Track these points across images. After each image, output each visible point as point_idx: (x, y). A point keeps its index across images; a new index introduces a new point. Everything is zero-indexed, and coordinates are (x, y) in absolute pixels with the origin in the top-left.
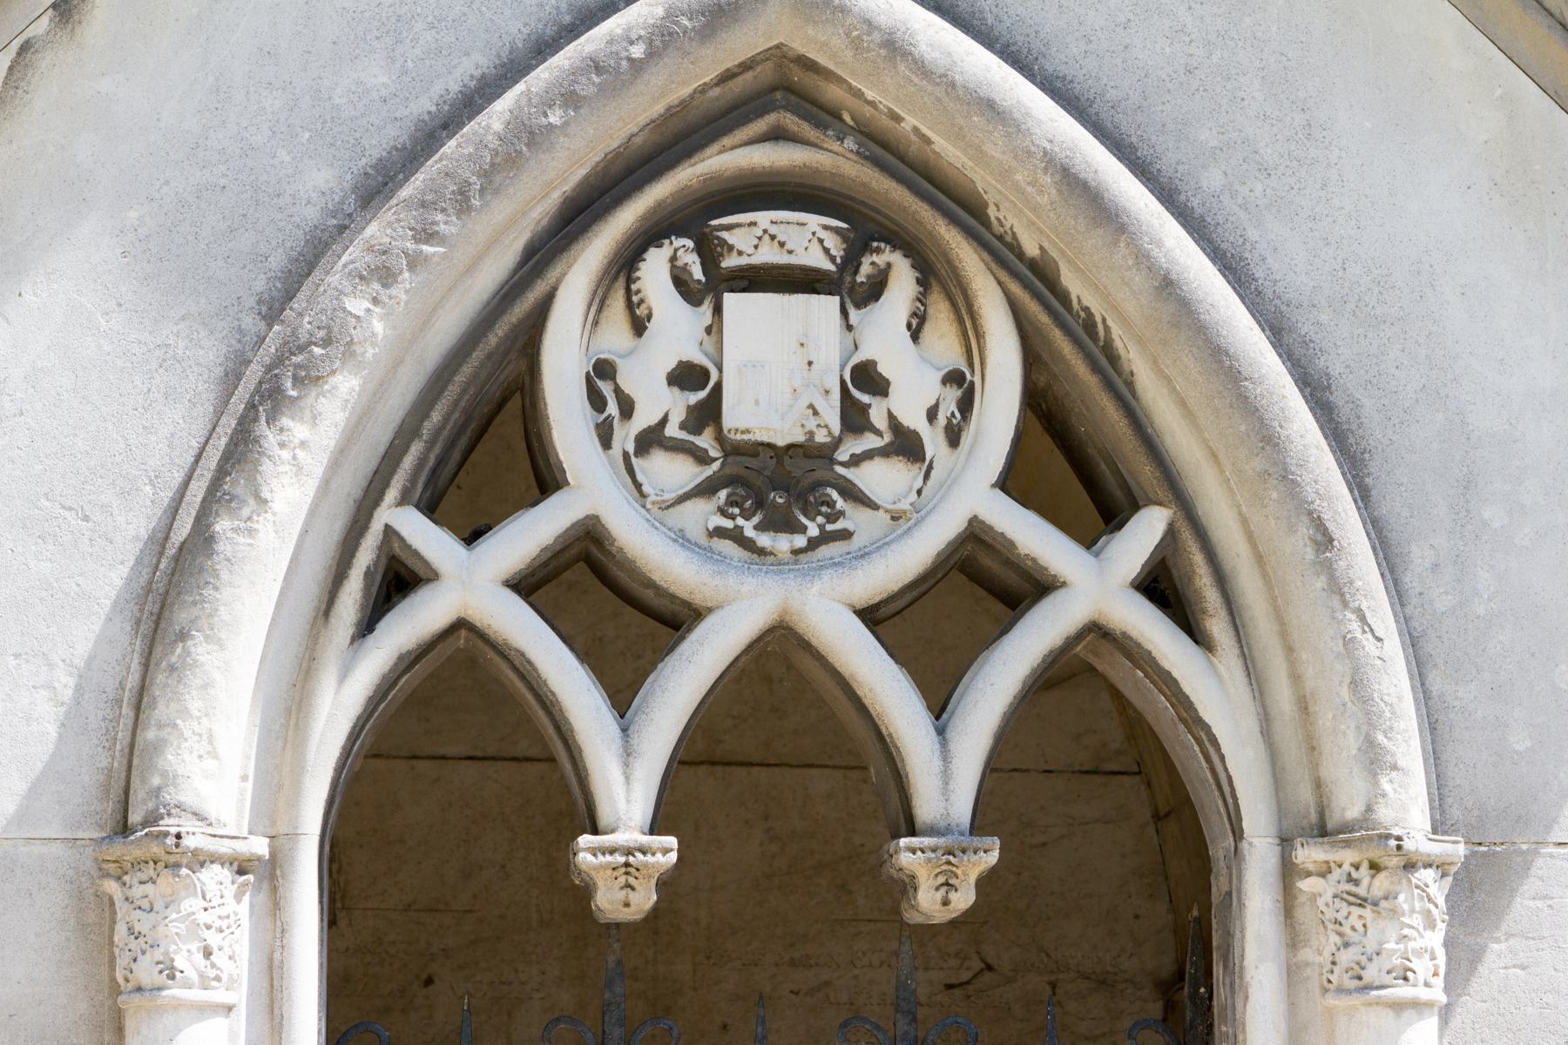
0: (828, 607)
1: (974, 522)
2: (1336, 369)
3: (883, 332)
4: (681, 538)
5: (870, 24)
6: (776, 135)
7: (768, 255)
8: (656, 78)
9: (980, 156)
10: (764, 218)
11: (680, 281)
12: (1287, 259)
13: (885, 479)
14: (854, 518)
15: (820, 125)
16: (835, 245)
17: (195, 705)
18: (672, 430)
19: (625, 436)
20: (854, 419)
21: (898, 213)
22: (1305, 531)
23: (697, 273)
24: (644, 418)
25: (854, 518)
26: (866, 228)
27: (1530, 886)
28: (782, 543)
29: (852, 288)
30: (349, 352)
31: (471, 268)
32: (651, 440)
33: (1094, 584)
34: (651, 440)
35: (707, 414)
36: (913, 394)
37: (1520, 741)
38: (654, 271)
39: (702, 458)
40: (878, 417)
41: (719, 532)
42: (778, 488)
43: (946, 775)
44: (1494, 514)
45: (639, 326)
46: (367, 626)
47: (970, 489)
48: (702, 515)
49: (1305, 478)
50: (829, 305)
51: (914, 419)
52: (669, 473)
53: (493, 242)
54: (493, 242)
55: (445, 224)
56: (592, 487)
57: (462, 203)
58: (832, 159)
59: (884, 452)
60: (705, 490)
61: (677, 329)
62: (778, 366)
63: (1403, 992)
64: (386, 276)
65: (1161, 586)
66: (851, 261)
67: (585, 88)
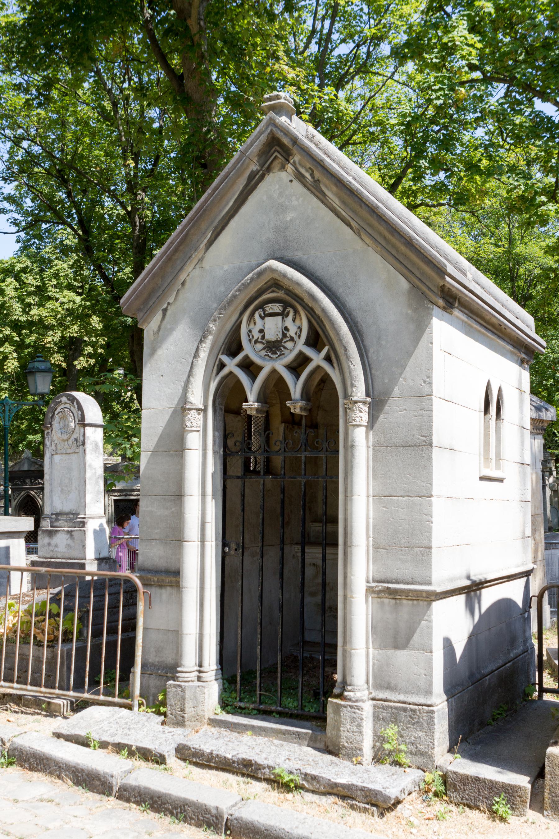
0: (280, 366)
1: (300, 351)
2: (359, 320)
3: (289, 322)
4: (260, 357)
5: (281, 273)
6: (273, 292)
7: (271, 311)
8: (252, 286)
9: (240, 303)
10: (270, 305)
11: (260, 316)
12: (352, 302)
13: (289, 345)
14: (285, 352)
15: (279, 289)
16: (281, 308)
17: (190, 387)
18: (259, 340)
19: (253, 342)
20: (284, 335)
21: (291, 301)
22: (343, 348)
23: (263, 315)
24: (255, 338)
25: (285, 352)
26: (286, 304)
27: (387, 405)
28: (274, 356)
29: (283, 315)
30: (210, 333)
31: (230, 317)
32: (256, 342)
33: (317, 359)
34: (256, 342)
35: (263, 337)
36: (292, 332)
37: (386, 381)
38: (257, 315)
39: (263, 344)
40: (288, 335)
41: (266, 355)
42: (274, 347)
43: (295, 392)
44: (383, 343)
45: (255, 324)
46: (218, 374)
47: (301, 346)
48: (263, 353)
49: (343, 340)
50: (280, 318)
51: (293, 335)
52: (259, 346)
53: (233, 313)
54: (233, 313)
55: (223, 312)
56: (248, 350)
57: (225, 308)
58: (280, 294)
59: (289, 340)
60: (264, 349)
61: (259, 323)
62: (272, 327)
63: (354, 423)
64: (215, 320)
65: (328, 359)
66: (284, 311)
67: (241, 288)
